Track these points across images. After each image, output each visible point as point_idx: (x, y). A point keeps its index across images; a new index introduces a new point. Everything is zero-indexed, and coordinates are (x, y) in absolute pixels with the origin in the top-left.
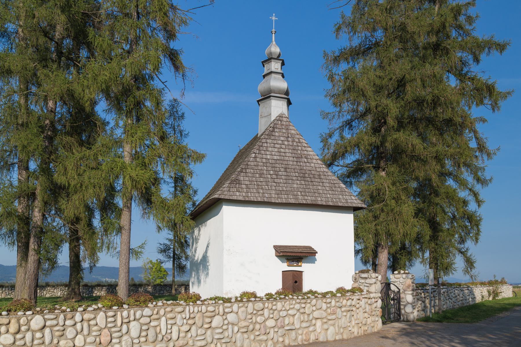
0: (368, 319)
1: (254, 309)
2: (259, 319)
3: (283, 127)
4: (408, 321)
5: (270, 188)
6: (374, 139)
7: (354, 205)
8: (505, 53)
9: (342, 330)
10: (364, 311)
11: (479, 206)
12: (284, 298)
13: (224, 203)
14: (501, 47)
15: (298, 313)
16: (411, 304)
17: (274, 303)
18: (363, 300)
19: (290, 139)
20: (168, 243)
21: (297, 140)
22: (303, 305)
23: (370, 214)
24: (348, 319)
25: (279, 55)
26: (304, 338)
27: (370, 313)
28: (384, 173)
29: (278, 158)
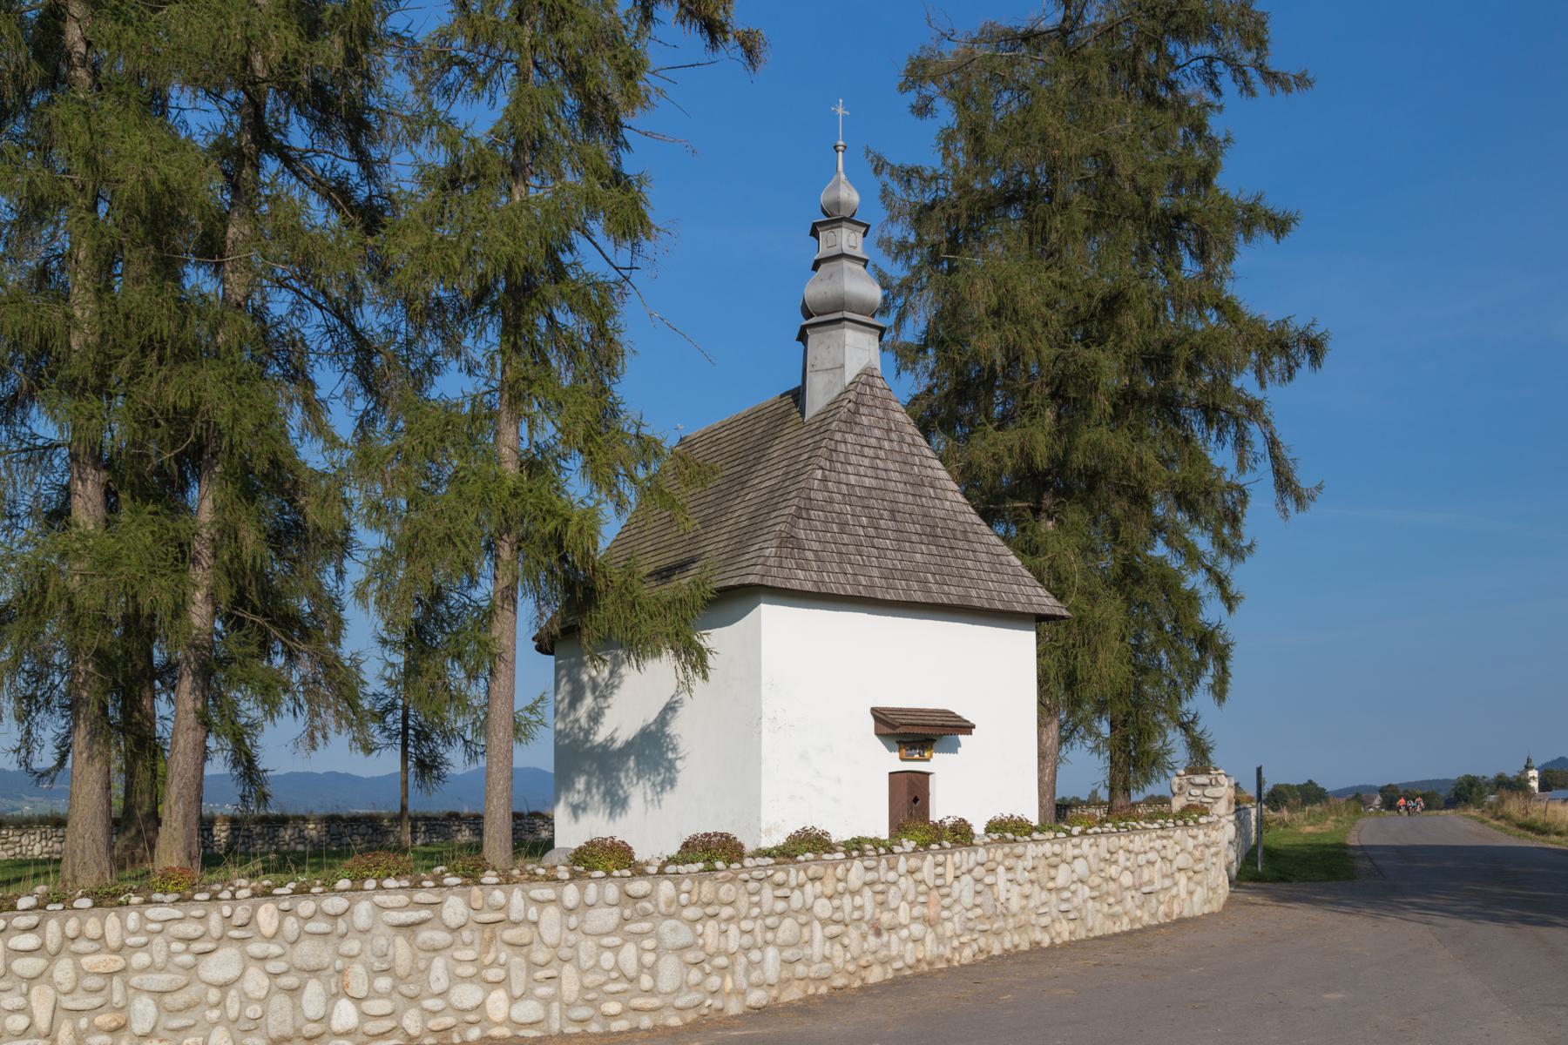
7: (1039, 610)
8: (1286, 240)
11: (1230, 609)
13: (763, 598)
14: (1279, 226)
19: (894, 436)
29: (874, 483)
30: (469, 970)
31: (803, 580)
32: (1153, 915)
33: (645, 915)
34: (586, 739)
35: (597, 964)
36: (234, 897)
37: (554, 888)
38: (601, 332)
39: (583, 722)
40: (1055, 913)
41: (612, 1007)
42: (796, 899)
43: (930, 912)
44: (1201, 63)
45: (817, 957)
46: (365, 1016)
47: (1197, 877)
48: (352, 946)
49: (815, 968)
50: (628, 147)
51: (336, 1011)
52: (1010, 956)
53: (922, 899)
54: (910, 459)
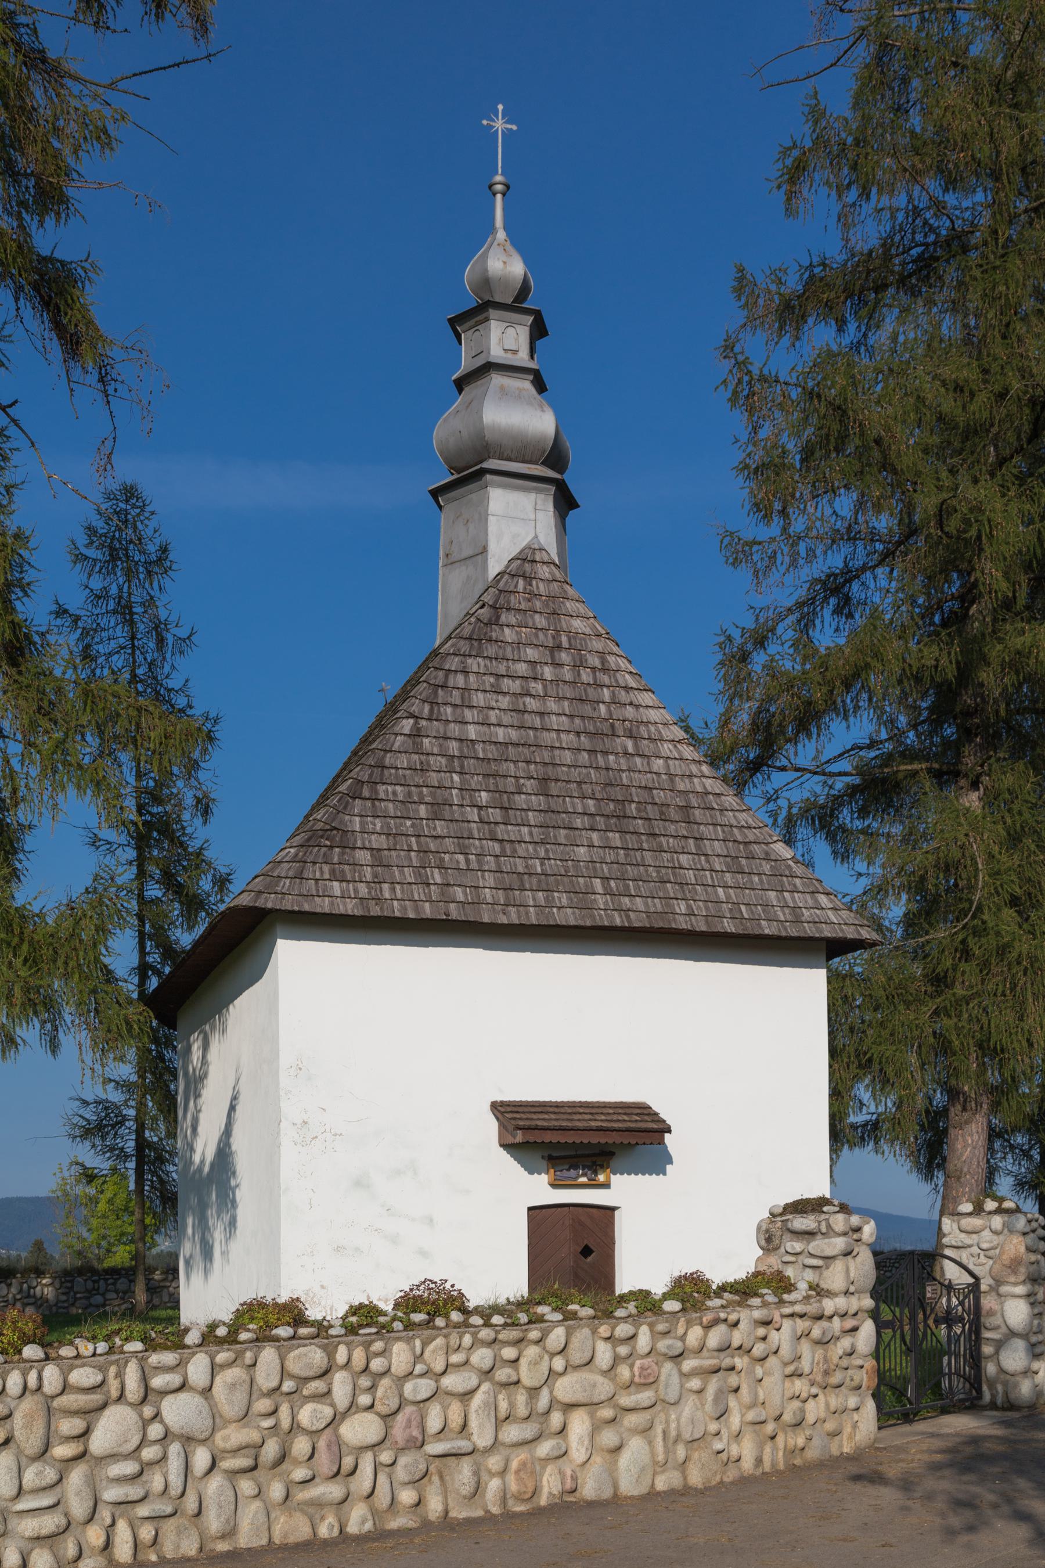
0: (811, 1404)
1: (284, 1373)
2: (307, 1415)
3: (538, 604)
4: (1010, 1406)
5: (474, 865)
6: (931, 654)
7: (827, 932)
9: (681, 1452)
10: (790, 1369)
12: (429, 1323)
13: (279, 929)
15: (485, 1387)
16: (1024, 1336)
17: (378, 1346)
18: (787, 1324)
19: (564, 657)
20: (116, 1096)
21: (595, 661)
22: (509, 1353)
23: (917, 970)
24: (709, 1407)
25: (524, 290)
26: (513, 1486)
27: (819, 1378)
28: (974, 796)
29: (514, 735)
31: (338, 898)
54: (592, 693)
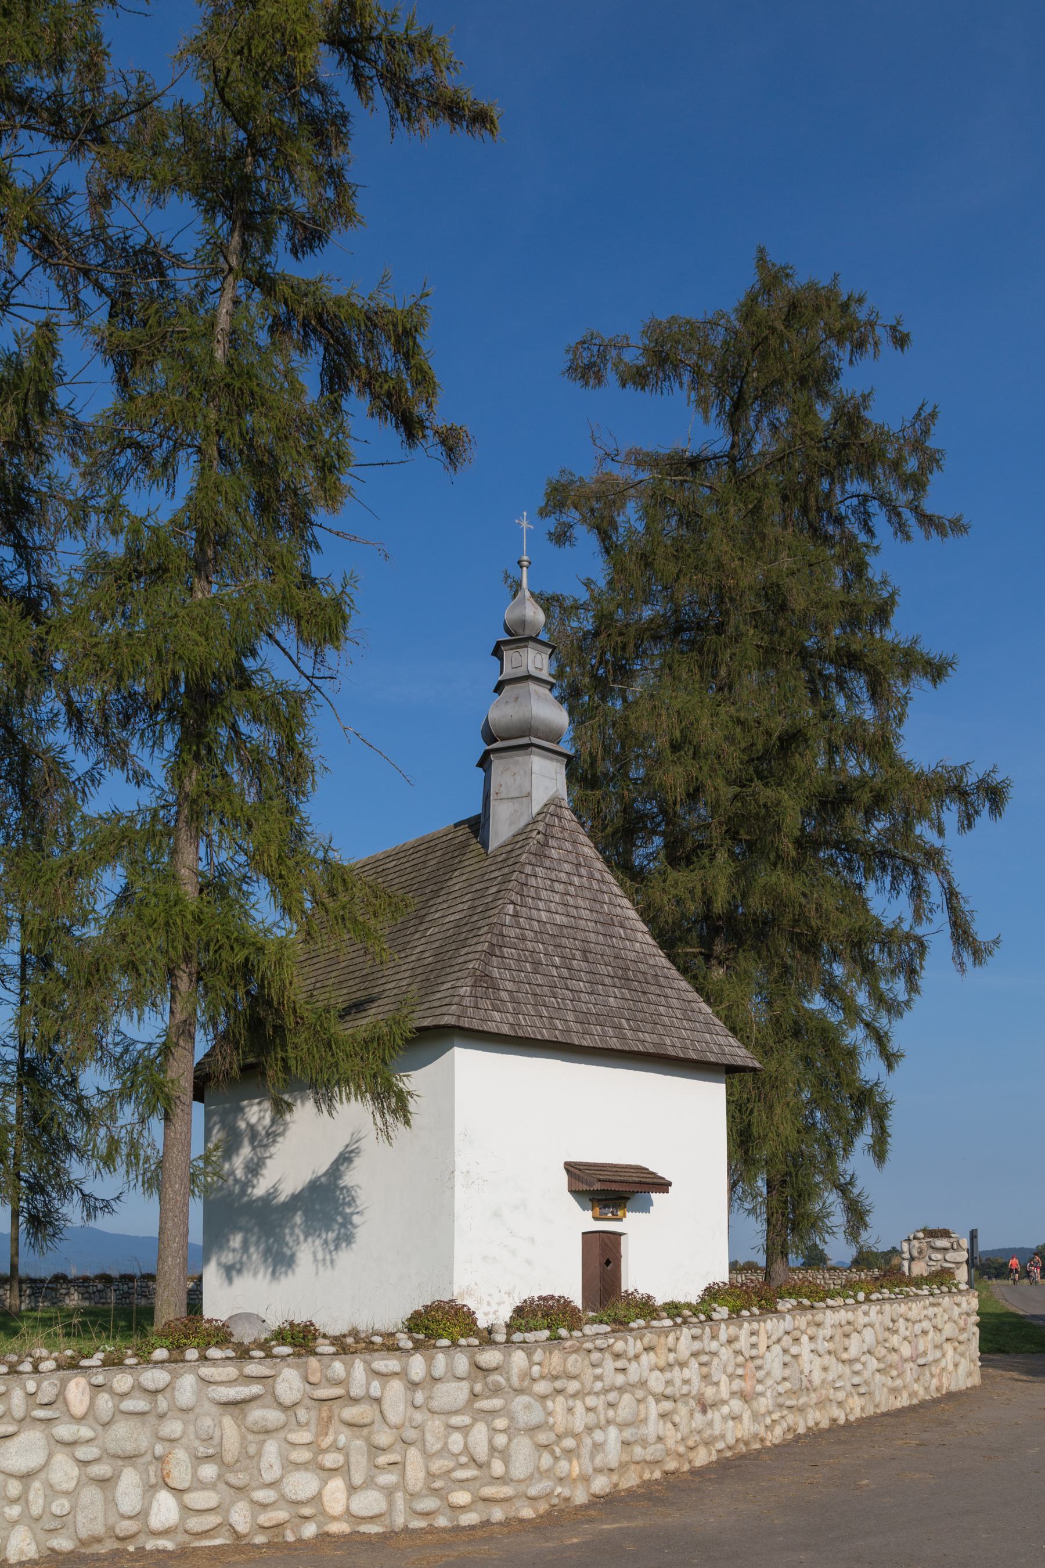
8: (942, 686)
11: (890, 1066)
19: (583, 871)
29: (565, 920)
30: (304, 1455)
31: (499, 1023)
32: (927, 1389)
33: (496, 1391)
34: (243, 1192)
35: (445, 1448)
36: (36, 1370)
37: (399, 1359)
38: (290, 746)
39: (239, 1173)
40: (849, 1387)
41: (461, 1497)
42: (634, 1372)
43: (746, 1386)
44: (855, 501)
45: (652, 1438)
46: (187, 1510)
47: (962, 1348)
48: (174, 1427)
49: (651, 1449)
50: (318, 547)
51: (155, 1504)
52: (815, 1434)
53: (740, 1371)
